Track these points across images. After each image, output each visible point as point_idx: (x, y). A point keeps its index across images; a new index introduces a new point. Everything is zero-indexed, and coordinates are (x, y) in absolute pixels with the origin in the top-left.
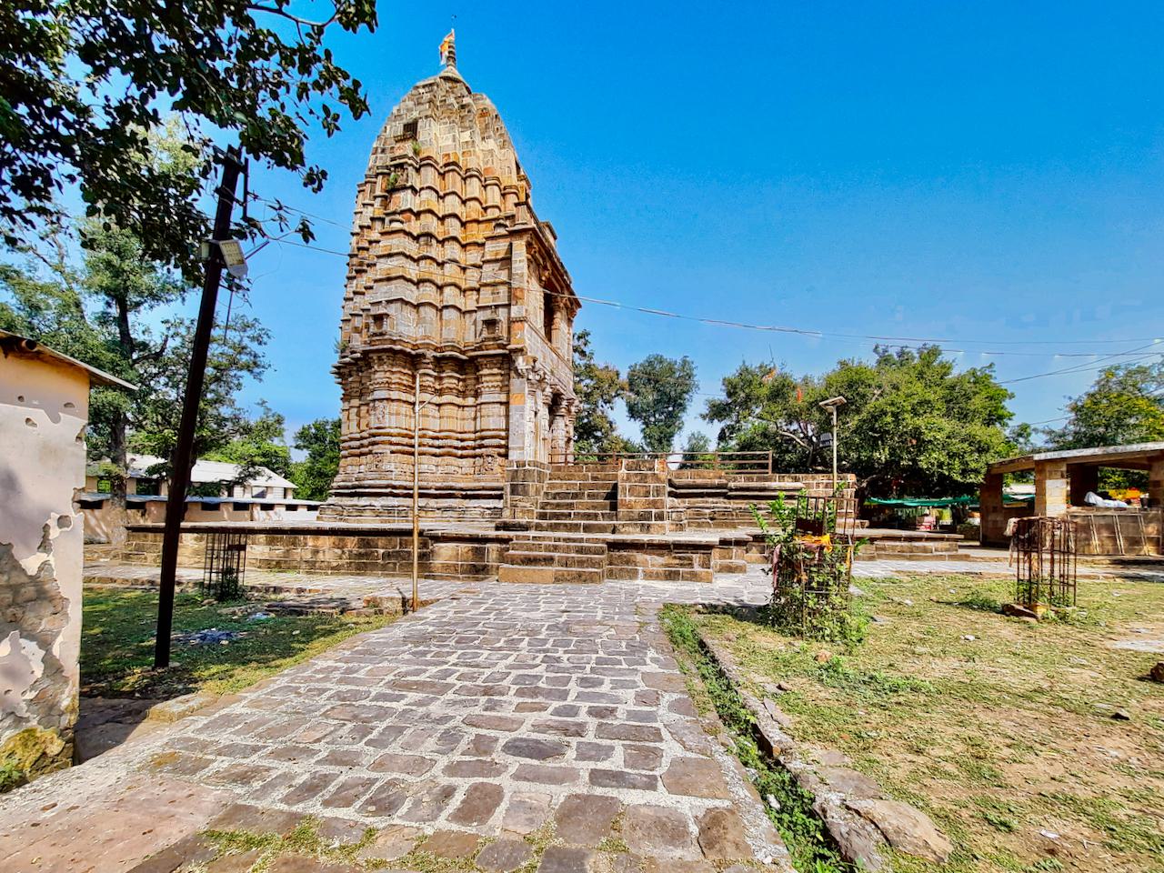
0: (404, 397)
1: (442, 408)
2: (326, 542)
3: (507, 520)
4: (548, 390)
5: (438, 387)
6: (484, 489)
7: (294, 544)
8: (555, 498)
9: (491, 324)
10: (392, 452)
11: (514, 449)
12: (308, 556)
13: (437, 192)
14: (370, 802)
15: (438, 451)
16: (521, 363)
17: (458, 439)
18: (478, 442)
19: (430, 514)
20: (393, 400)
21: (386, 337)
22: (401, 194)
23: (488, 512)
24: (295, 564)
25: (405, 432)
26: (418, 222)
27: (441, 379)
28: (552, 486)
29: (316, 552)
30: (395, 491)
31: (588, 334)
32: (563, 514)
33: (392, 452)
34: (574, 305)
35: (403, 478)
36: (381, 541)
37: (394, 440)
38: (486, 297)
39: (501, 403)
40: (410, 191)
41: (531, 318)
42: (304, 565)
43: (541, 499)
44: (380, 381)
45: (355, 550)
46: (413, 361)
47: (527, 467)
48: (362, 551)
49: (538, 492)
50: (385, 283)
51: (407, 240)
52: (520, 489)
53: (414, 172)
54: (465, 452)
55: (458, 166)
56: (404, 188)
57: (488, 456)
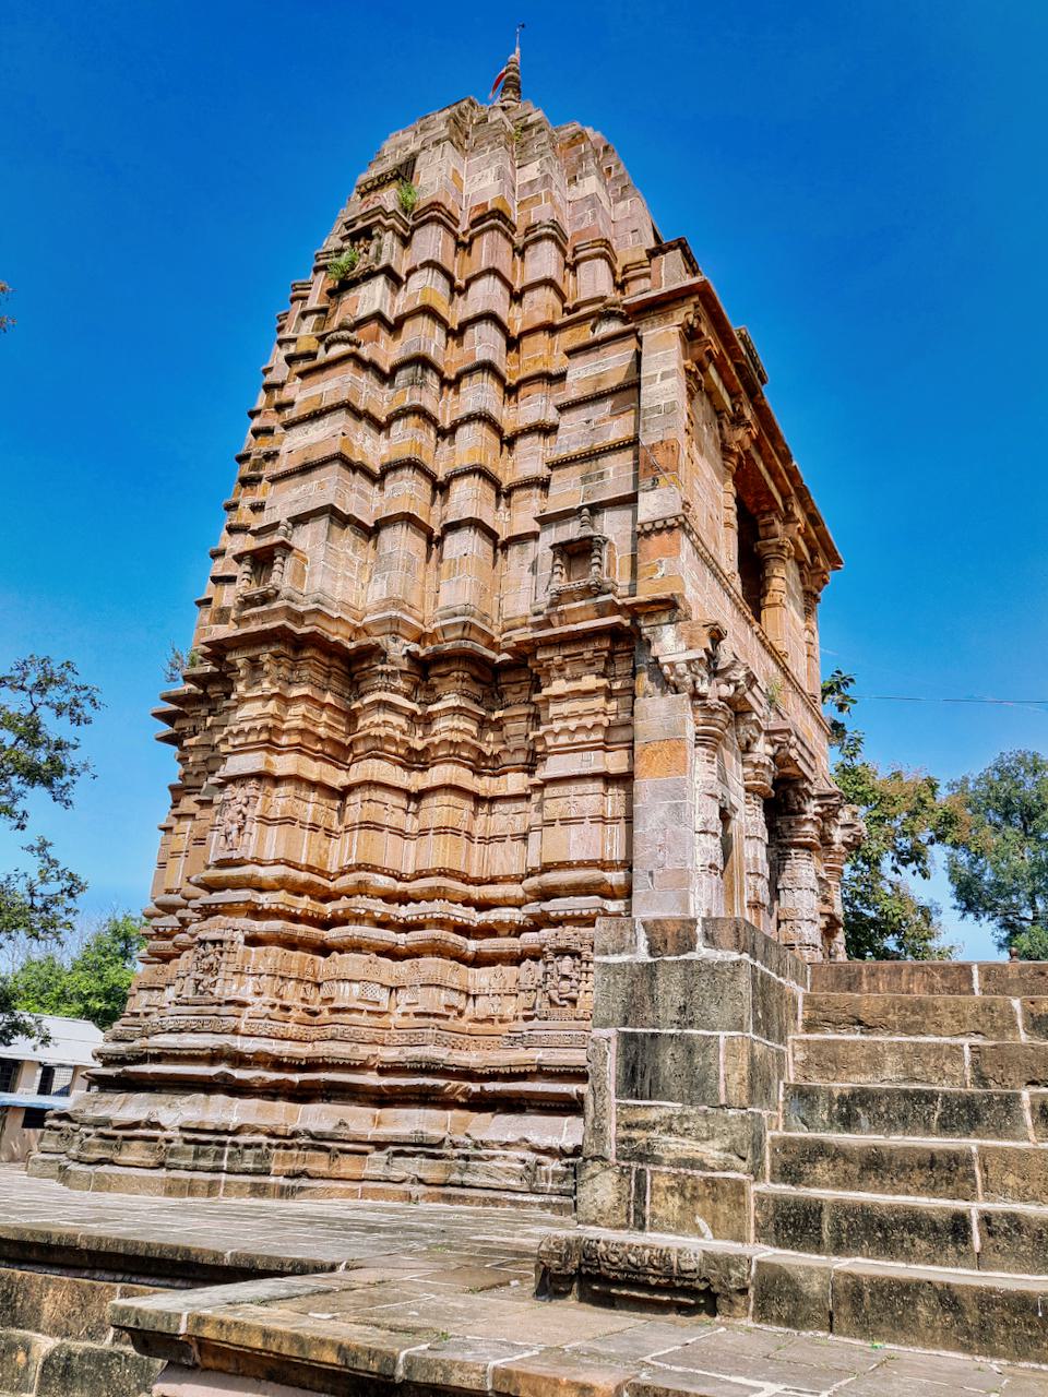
0: (315, 770)
1: (425, 803)
3: (604, 1236)
4: (762, 750)
5: (419, 745)
6: (542, 1072)
8: (847, 1121)
9: (576, 553)
10: (253, 941)
13: (449, 276)
14: (765, 979)
15: (403, 939)
16: (670, 645)
17: (467, 902)
18: (534, 908)
19: (347, 1166)
20: (277, 781)
22: (363, 291)
23: (554, 1165)
25: (304, 876)
26: (398, 342)
27: (428, 721)
28: (827, 1059)
30: (240, 1074)
31: (848, 682)
32: (914, 1223)
33: (253, 941)
34: (819, 558)
35: (277, 1027)
36: (53, 1293)
37: (265, 900)
38: (568, 491)
39: (608, 779)
40: (381, 279)
41: (701, 523)
43: (779, 1124)
44: (246, 726)
46: (351, 665)
47: (702, 951)
49: (759, 1081)
50: (297, 479)
51: (366, 380)
52: (668, 1061)
53: (396, 245)
54: (488, 945)
55: (505, 219)
56: (369, 275)
57: (561, 952)
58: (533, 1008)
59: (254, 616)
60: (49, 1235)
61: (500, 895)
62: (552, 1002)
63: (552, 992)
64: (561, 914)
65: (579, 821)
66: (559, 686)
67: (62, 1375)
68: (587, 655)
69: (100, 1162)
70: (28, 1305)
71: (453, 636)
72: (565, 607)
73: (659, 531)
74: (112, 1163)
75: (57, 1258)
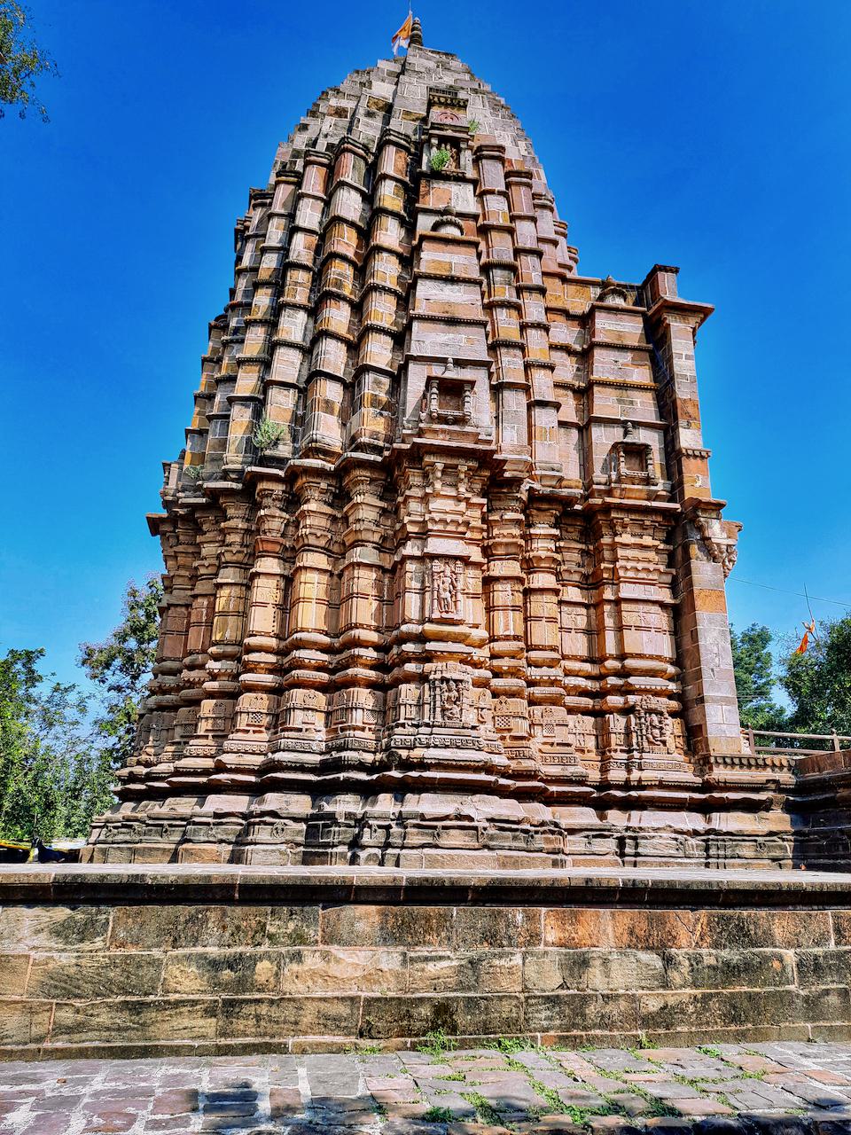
2: (604, 928)
6: (662, 785)
7: (491, 937)
11: (715, 700)
12: (549, 978)
21: (467, 429)
24: (506, 1009)
29: (579, 964)
42: (542, 1015)
45: (709, 956)
48: (731, 955)
50: (442, 326)
59: (443, 431)
60: (710, 883)
61: (577, 669)
64: (659, 688)
65: (648, 629)
66: (626, 538)
67: (814, 971)
68: (647, 523)
69: (423, 846)
70: (760, 933)
71: (548, 483)
72: (628, 486)
73: (695, 457)
74: (437, 847)
75: (775, 899)
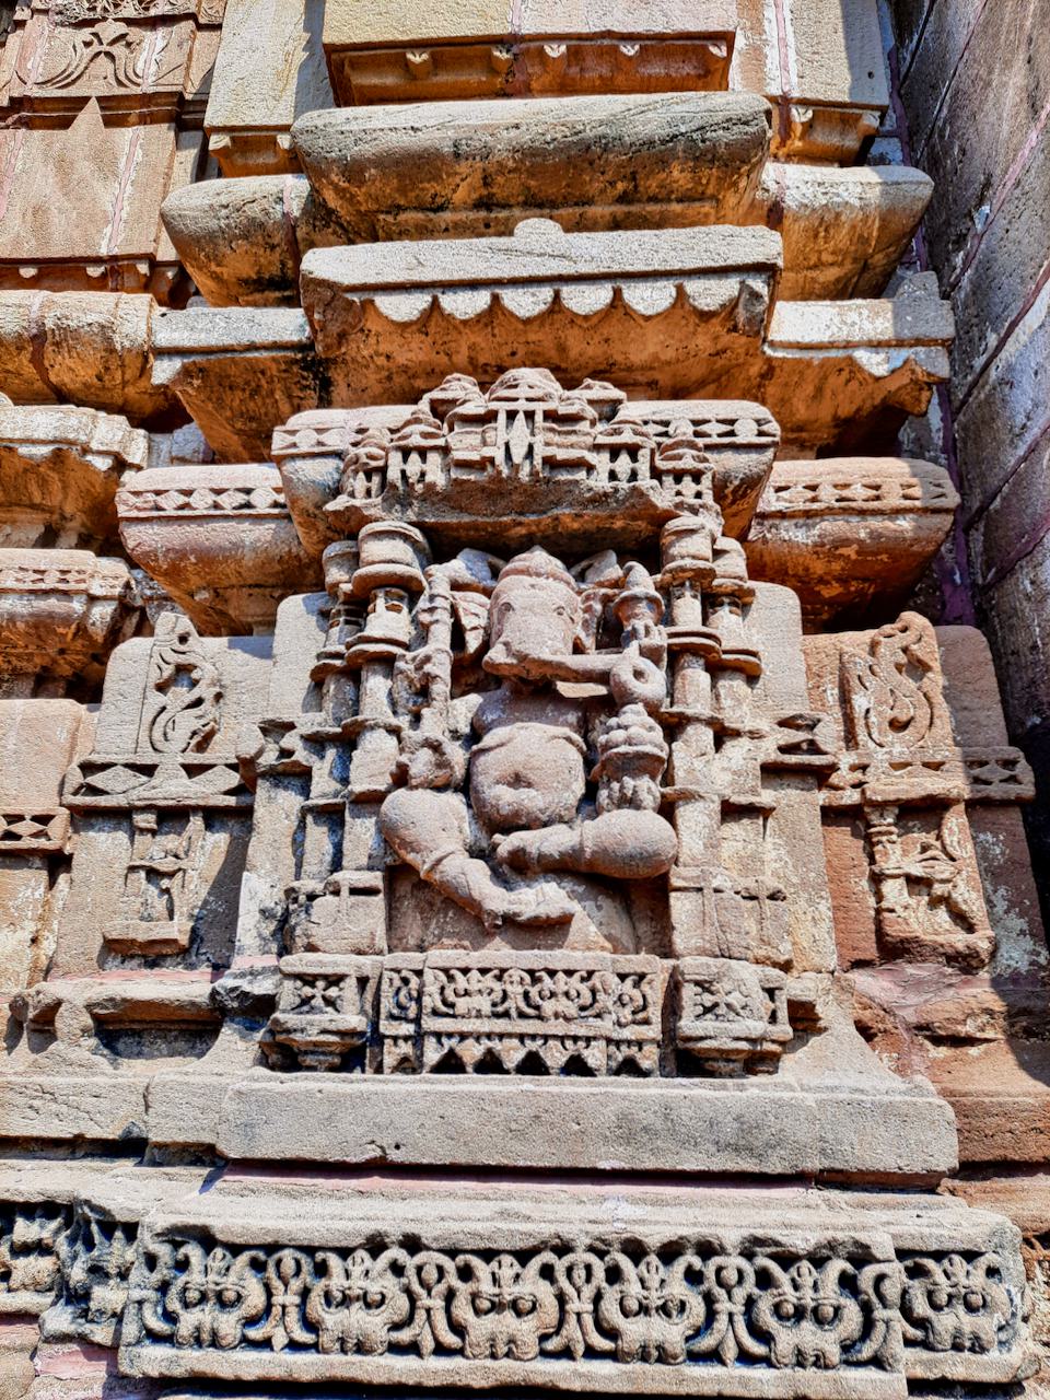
57: (482, 523)
58: (211, 937)
62: (404, 881)
63: (408, 806)
